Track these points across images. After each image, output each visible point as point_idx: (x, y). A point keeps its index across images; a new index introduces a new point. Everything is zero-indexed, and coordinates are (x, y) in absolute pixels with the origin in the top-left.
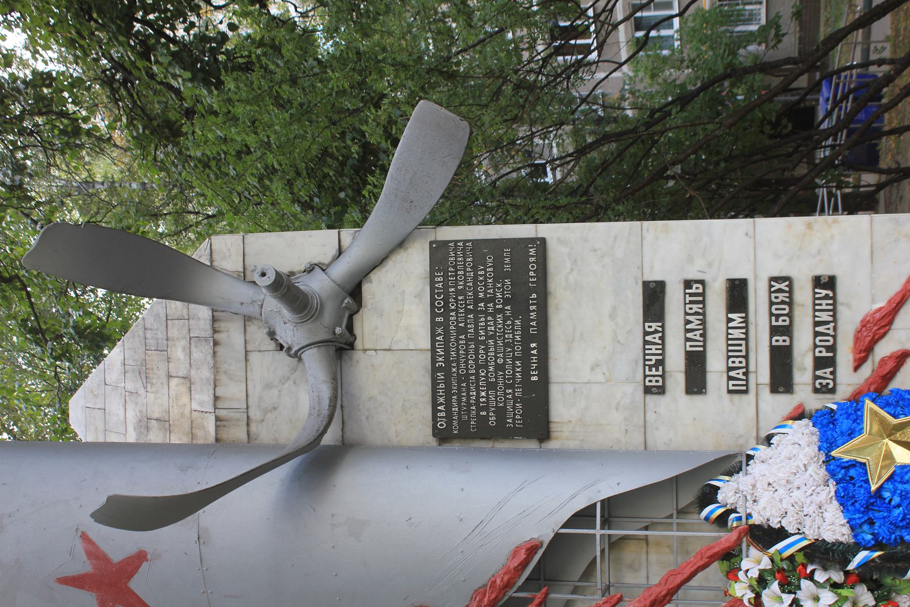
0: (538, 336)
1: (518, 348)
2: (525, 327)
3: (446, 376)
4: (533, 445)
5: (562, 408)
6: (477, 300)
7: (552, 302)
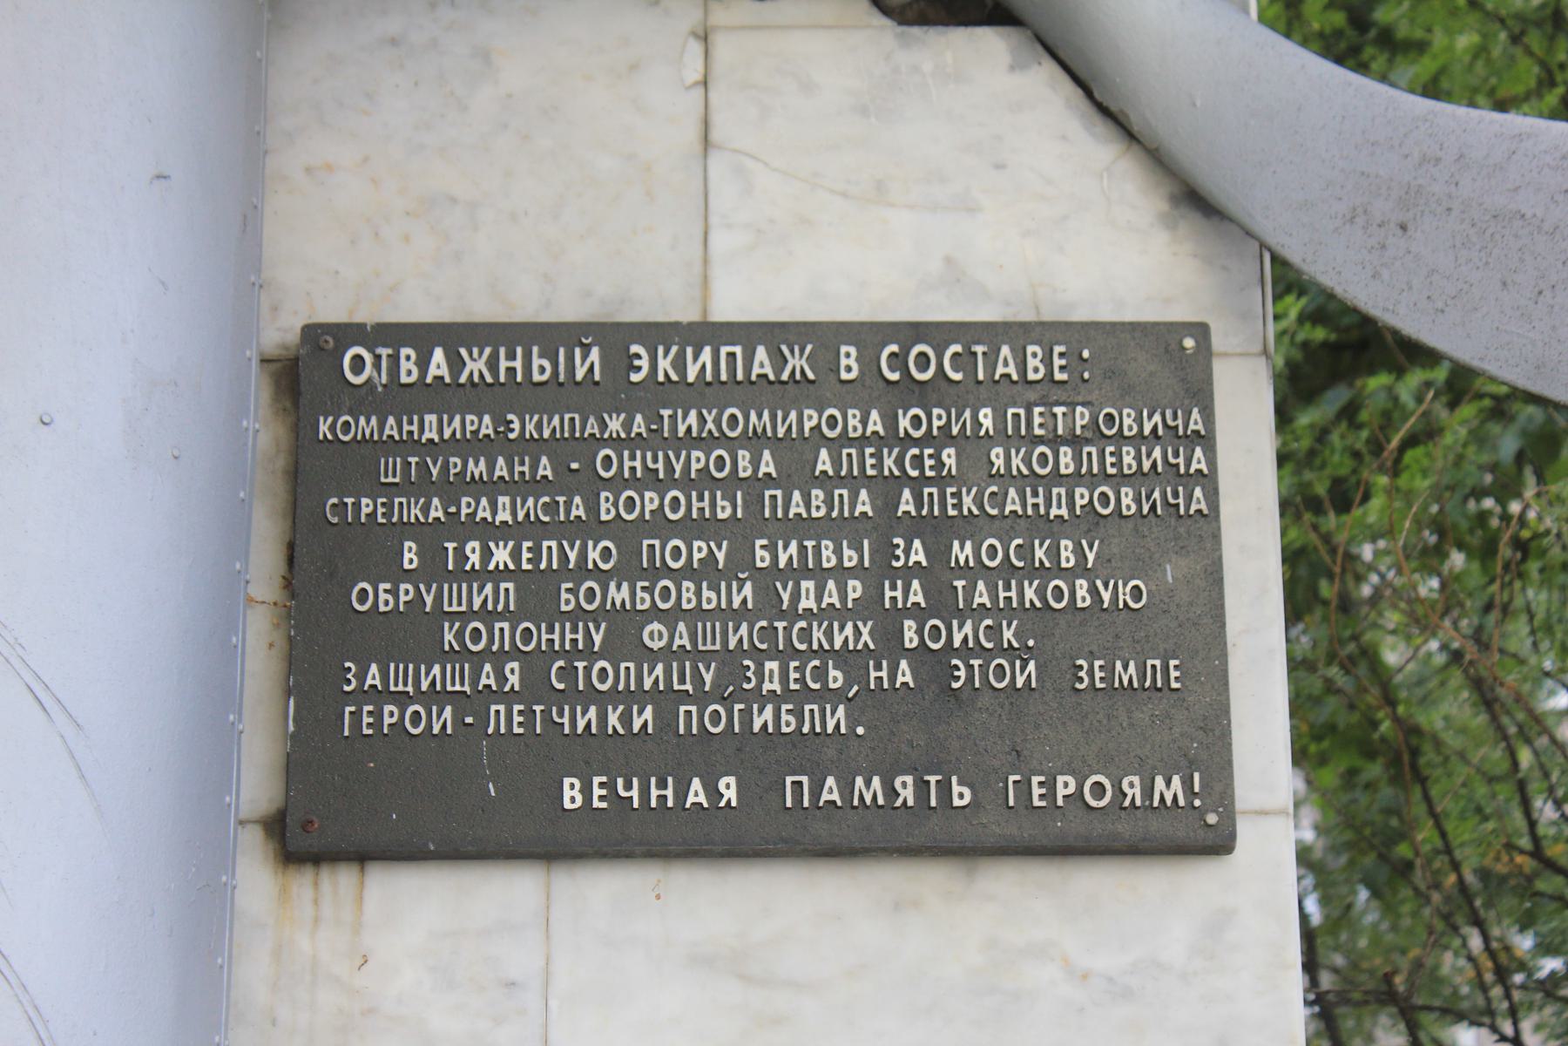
0: (773, 824)
1: (715, 719)
2: (808, 751)
3: (582, 391)
4: (257, 784)
5: (424, 924)
6: (937, 531)
7: (929, 881)
